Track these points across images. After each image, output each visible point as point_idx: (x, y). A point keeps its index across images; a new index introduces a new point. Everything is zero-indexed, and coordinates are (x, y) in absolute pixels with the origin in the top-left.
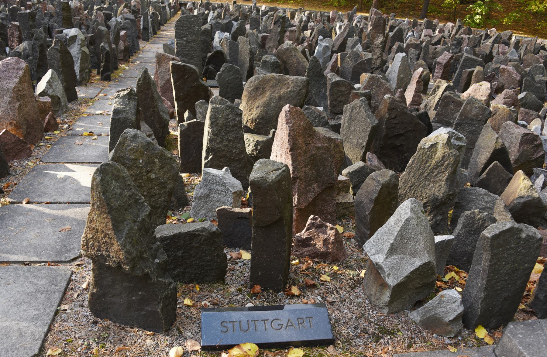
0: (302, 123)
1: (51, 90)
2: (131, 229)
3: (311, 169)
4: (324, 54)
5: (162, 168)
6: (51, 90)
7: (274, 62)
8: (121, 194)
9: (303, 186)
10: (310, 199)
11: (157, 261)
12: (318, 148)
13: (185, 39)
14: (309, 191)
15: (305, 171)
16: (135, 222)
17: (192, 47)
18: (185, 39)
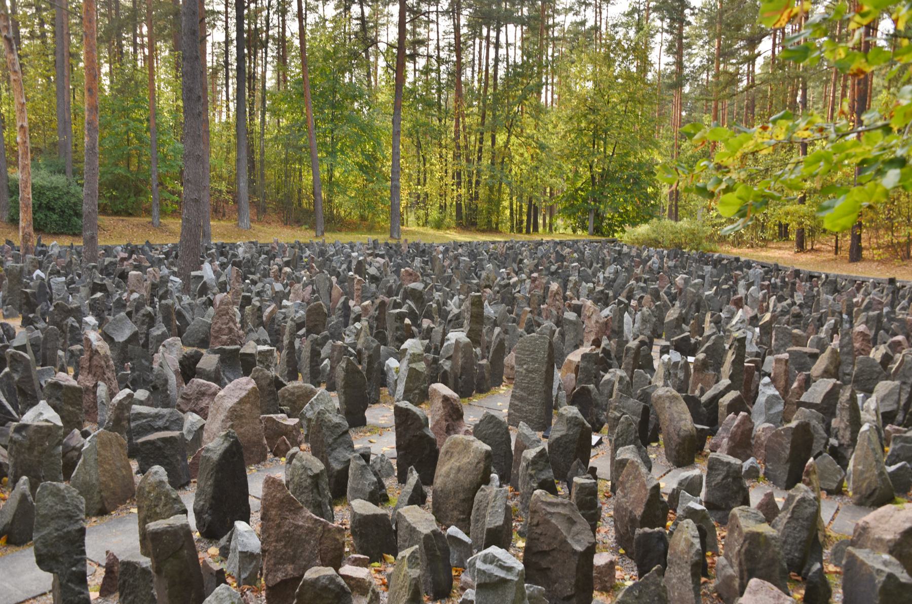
0: (278, 495)
1: (311, 413)
2: (49, 533)
3: (285, 546)
4: (769, 409)
5: (165, 505)
6: (311, 413)
7: (572, 418)
8: (52, 507)
9: (272, 562)
10: (279, 580)
11: (74, 569)
12: (298, 527)
13: (525, 367)
14: (279, 570)
15: (275, 546)
16: (57, 530)
17: (533, 379)
18: (525, 367)
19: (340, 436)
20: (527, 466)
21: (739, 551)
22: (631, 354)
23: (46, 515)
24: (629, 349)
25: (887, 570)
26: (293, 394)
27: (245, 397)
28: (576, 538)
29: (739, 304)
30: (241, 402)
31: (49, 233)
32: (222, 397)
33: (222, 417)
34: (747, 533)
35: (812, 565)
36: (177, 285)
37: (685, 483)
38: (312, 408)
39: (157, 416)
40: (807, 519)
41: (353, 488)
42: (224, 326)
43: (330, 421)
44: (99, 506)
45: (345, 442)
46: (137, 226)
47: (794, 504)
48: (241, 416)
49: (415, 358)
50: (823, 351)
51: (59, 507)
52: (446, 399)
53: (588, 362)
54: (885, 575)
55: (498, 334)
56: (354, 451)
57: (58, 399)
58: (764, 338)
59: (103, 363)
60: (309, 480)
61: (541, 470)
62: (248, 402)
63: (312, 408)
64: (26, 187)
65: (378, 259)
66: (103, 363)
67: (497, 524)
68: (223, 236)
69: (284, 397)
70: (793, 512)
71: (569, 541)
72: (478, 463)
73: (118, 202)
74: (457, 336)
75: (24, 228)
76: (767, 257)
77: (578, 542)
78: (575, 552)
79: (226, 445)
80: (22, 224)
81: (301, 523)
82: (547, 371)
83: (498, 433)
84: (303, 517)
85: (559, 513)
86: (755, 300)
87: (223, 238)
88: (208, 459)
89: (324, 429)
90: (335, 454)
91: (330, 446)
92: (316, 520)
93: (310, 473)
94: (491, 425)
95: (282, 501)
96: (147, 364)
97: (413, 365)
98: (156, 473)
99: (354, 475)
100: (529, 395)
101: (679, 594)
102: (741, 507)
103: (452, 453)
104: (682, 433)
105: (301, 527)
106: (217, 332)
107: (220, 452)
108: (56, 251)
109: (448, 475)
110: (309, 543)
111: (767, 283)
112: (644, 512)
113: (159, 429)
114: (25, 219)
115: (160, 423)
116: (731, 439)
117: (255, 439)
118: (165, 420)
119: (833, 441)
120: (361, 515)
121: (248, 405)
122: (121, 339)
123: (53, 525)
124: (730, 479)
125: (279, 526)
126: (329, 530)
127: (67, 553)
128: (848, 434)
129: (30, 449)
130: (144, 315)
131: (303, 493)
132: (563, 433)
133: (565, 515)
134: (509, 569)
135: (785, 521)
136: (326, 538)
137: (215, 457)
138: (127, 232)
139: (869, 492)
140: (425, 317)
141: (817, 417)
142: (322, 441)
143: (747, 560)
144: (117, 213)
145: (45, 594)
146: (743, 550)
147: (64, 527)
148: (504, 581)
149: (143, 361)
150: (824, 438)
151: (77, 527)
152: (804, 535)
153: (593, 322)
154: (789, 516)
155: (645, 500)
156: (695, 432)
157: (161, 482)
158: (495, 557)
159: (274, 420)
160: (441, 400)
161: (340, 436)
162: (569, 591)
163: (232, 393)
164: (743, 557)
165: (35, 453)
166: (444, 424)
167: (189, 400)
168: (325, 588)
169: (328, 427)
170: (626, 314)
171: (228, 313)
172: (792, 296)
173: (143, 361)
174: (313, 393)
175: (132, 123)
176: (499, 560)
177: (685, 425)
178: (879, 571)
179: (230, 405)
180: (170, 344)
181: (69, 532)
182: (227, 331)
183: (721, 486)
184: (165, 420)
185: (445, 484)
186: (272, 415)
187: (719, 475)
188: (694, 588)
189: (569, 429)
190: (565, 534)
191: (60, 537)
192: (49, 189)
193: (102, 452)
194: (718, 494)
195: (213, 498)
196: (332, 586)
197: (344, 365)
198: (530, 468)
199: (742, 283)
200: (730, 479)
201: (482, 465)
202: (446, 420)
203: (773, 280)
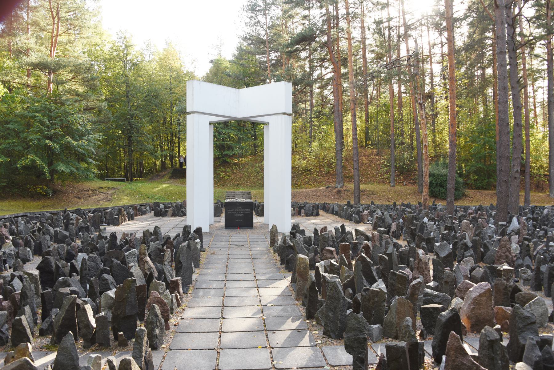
2: (351, 336)
5: (408, 338)
12: (463, 364)
19: (528, 324)
23: (351, 327)
26: (524, 297)
27: (483, 293)
30: (480, 295)
31: (440, 199)
32: (471, 291)
33: (469, 302)
36: (492, 229)
38: (530, 307)
39: (436, 296)
41: (526, 356)
43: (522, 314)
44: (395, 334)
46: (488, 195)
48: (480, 304)
51: (357, 325)
57: (394, 280)
59: (423, 266)
60: (487, 343)
62: (485, 296)
63: (530, 307)
64: (426, 175)
66: (423, 266)
68: (539, 201)
69: (518, 298)
73: (478, 182)
75: (424, 196)
76: (314, 219)
79: (451, 315)
80: (424, 194)
81: (465, 362)
84: (467, 359)
87: (539, 203)
88: (440, 320)
89: (517, 318)
90: (523, 334)
91: (520, 329)
93: (488, 338)
95: (457, 348)
96: (441, 269)
98: (407, 321)
99: (528, 348)
100: (492, 295)
105: (465, 364)
106: (499, 257)
107: (447, 318)
108: (440, 207)
113: (435, 303)
114: (425, 191)
115: (437, 300)
117: (488, 318)
118: (440, 299)
121: (485, 298)
122: (443, 256)
123: (353, 333)
125: (454, 361)
127: (357, 347)
129: (369, 300)
130: (462, 244)
131: (484, 349)
137: (444, 320)
138: (482, 199)
142: (515, 325)
144: (478, 188)
145: (326, 360)
147: (358, 335)
149: (439, 267)
151: (363, 336)
157: (408, 325)
159: (503, 310)
161: (528, 324)
163: (476, 290)
165: (371, 303)
167: (461, 291)
169: (520, 317)
171: (506, 247)
173: (439, 267)
174: (533, 297)
175: (487, 139)
179: (474, 296)
180: (467, 261)
181: (359, 338)
182: (504, 257)
184: (440, 299)
191: (355, 339)
192: (442, 176)
193: (399, 308)
195: (440, 341)
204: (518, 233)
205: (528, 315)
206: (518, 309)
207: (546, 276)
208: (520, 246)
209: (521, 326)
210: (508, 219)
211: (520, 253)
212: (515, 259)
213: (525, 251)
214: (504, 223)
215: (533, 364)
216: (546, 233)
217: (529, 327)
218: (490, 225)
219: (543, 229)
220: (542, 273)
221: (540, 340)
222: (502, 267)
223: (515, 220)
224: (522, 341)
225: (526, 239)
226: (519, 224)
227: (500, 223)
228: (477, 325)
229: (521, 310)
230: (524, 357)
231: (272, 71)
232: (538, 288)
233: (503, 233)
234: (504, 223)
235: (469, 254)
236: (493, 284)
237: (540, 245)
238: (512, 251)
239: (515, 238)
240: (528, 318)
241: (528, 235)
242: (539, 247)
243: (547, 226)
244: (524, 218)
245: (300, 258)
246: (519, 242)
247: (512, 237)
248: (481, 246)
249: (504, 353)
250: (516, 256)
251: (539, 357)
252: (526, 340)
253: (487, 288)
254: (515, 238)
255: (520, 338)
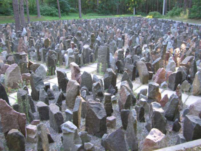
13: (101, 56)
19: (39, 81)
20: (94, 88)
21: (152, 117)
22: (134, 50)
24: (134, 49)
25: (196, 123)
26: (34, 66)
28: (100, 114)
29: (169, 34)
34: (154, 112)
35: (175, 119)
37: (142, 91)
40: (175, 104)
42: (21, 47)
45: (41, 82)
47: (172, 100)
49: (71, 54)
50: (190, 48)
52: (75, 67)
53: (120, 53)
54: (195, 125)
55: (97, 46)
56: (44, 85)
58: (175, 44)
61: (98, 89)
65: (73, 24)
67: (76, 111)
70: (171, 102)
71: (97, 116)
72: (76, 89)
74: (86, 46)
77: (101, 116)
78: (99, 119)
82: (107, 57)
83: (88, 77)
84: (12, 112)
85: (95, 107)
86: (174, 32)
89: (33, 79)
90: (38, 86)
92: (16, 113)
94: (86, 75)
97: (70, 56)
101: (131, 132)
102: (153, 102)
103: (70, 86)
104: (73, 96)
105: (12, 115)
109: (68, 93)
110: (14, 120)
111: (179, 27)
112: (125, 103)
116: (158, 76)
119: (189, 76)
120: (39, 107)
124: (155, 90)
126: (20, 116)
128: (193, 74)
132: (108, 77)
133: (96, 107)
134: (72, 129)
135: (169, 104)
136: (20, 118)
139: (197, 92)
140: (80, 41)
141: (185, 69)
143: (154, 120)
146: (153, 117)
148: (70, 133)
150: (186, 75)
152: (175, 109)
153: (127, 40)
154: (170, 103)
155: (126, 100)
156: (148, 75)
158: (68, 125)
160: (73, 67)
161: (39, 81)
162: (98, 130)
164: (153, 119)
166: (75, 74)
168: (14, 136)
170: (137, 38)
172: (185, 31)
176: (69, 126)
177: (145, 72)
178: (194, 123)
179: (10, 72)
183: (153, 92)
185: (68, 96)
186: (25, 74)
187: (152, 89)
188: (134, 131)
189: (109, 75)
190: (96, 114)
194: (151, 95)
196: (17, 136)
197: (47, 58)
198: (95, 89)
199: (172, 27)
200: (155, 90)
201: (77, 90)
202: (75, 73)
203: (181, 27)
204: (27, 35)
205: (38, 76)
206: (33, 74)
207: (42, 54)
208: (29, 41)
209: (36, 82)
210: (21, 29)
211: (29, 44)
212: (27, 48)
213: (31, 43)
214: (20, 31)
215: (44, 100)
216: (39, 34)
217: (39, 82)
218: (13, 33)
219: (37, 32)
220: (40, 53)
221: (45, 87)
222: (22, 54)
223: (24, 29)
224: (38, 90)
225: (31, 38)
226: (27, 31)
227: (18, 31)
228: (15, 87)
229: (35, 75)
230: (40, 98)
231: (19, 46)
232: (39, 60)
233: (20, 36)
234: (20, 31)
235: (5, 49)
236: (19, 63)
237: (37, 40)
238: (25, 44)
239: (26, 38)
240: (38, 78)
241: (32, 35)
242: (37, 41)
243: (38, 30)
244: (28, 28)
245: (141, 95)
246: (28, 39)
247: (24, 38)
248: (10, 44)
249: (30, 99)
250: (27, 46)
251: (46, 96)
252: (39, 89)
253: (16, 66)
254: (26, 38)
255: (36, 88)
